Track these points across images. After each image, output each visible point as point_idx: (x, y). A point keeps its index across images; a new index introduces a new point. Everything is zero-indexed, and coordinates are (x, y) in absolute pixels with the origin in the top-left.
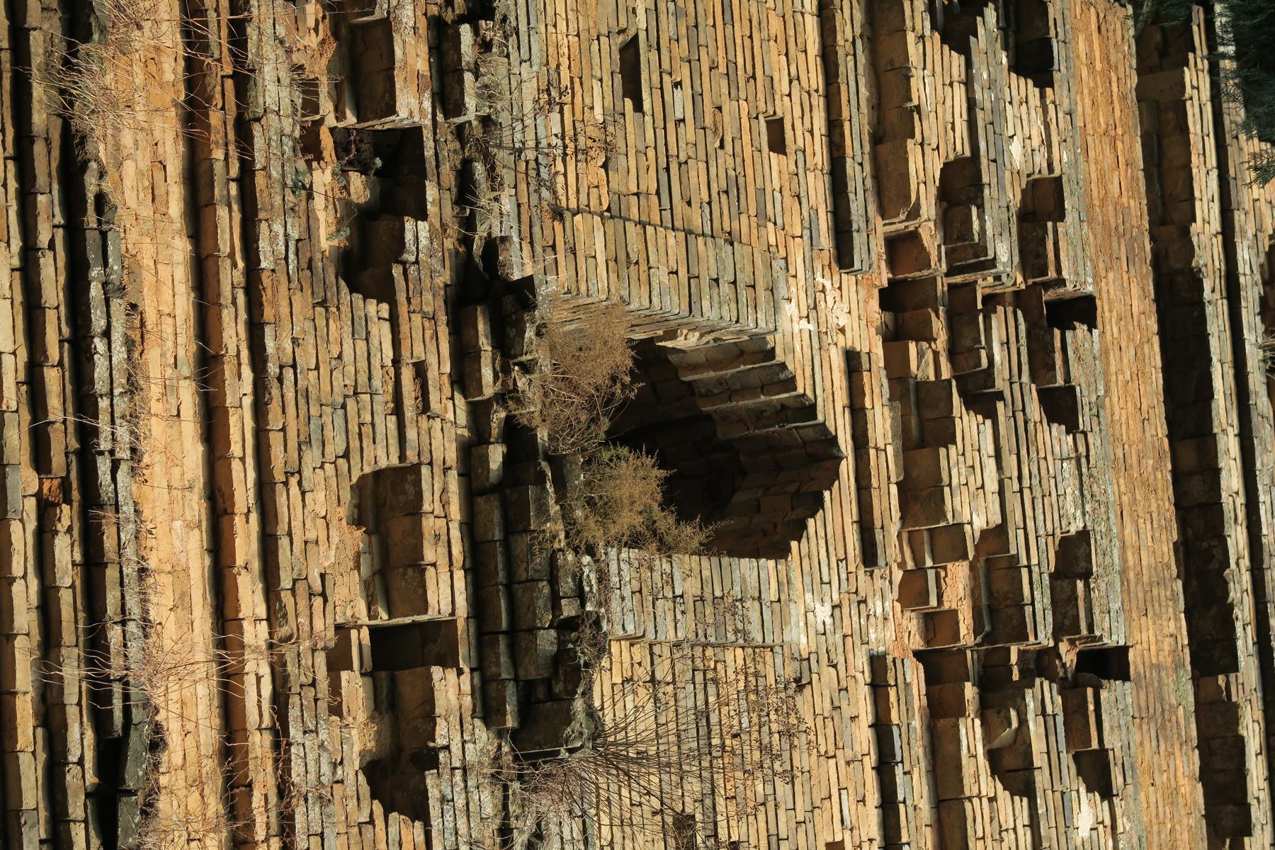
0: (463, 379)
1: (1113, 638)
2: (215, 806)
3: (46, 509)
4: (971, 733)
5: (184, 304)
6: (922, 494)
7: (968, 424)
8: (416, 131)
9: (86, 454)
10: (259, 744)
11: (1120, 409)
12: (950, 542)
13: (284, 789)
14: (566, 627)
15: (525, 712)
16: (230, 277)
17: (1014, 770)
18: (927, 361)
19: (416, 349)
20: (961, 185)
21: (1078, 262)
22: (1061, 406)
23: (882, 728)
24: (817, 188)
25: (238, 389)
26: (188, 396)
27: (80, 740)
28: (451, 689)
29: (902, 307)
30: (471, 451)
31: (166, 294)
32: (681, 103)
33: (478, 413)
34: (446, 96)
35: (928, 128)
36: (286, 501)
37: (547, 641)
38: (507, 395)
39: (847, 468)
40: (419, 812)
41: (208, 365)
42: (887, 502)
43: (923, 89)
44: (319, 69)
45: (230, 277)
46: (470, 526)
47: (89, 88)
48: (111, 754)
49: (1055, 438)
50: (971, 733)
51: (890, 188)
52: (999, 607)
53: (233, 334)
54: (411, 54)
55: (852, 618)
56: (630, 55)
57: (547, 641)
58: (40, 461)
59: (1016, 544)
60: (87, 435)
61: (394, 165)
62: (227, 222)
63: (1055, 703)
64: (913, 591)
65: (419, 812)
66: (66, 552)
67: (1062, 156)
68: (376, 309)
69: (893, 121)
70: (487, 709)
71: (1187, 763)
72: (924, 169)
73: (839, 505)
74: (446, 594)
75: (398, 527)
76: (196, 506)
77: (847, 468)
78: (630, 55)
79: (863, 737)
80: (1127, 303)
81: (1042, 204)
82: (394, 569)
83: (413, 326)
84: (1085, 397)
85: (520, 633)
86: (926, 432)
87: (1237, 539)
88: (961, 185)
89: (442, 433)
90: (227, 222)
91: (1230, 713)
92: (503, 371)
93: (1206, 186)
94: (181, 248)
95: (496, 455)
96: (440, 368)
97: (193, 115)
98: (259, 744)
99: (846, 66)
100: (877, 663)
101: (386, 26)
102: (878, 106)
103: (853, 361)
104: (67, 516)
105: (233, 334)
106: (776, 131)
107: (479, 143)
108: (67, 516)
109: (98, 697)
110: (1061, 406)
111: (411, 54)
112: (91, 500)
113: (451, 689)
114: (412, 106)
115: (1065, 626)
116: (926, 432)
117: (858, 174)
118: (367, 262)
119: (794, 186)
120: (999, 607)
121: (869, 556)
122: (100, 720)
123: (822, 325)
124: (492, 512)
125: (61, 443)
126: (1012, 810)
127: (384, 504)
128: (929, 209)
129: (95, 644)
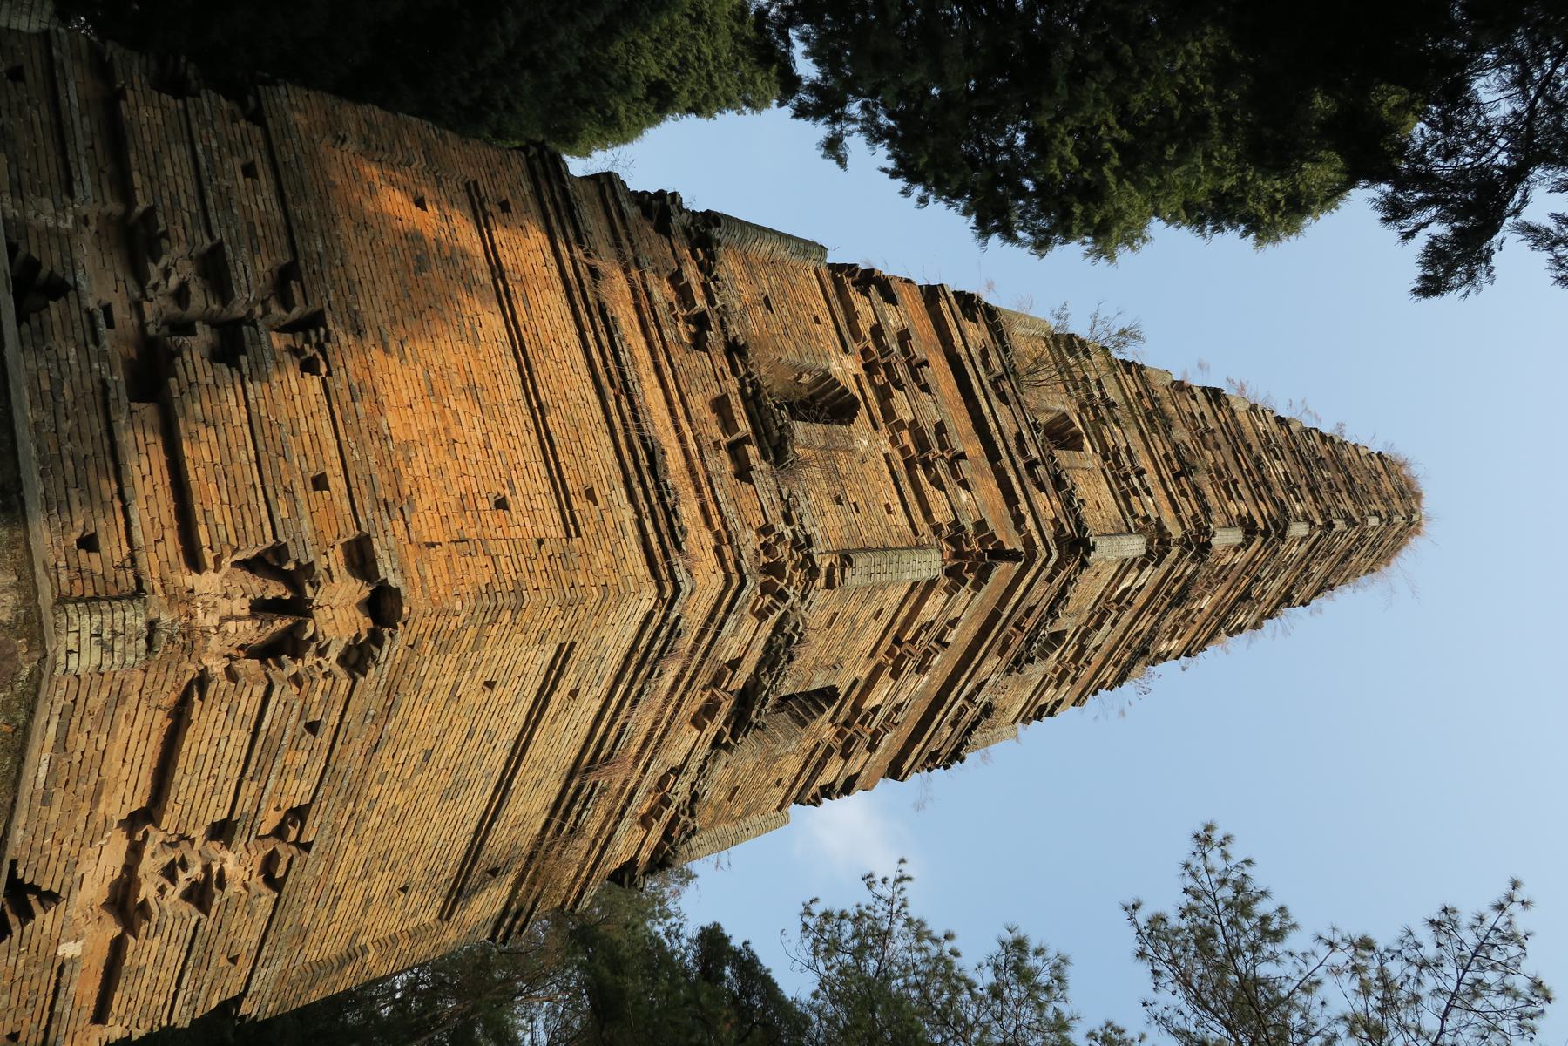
0: (735, 372)
1: (960, 449)
2: (689, 481)
3: (617, 398)
4: (921, 473)
5: (647, 354)
6: (888, 413)
7: (896, 393)
8: (704, 313)
9: (625, 382)
10: (697, 462)
11: (943, 388)
12: (901, 425)
13: (707, 471)
14: (780, 428)
15: (775, 455)
16: (658, 345)
17: (938, 484)
18: (880, 379)
19: (718, 364)
20: (877, 331)
21: (919, 352)
22: (925, 388)
23: (892, 473)
24: (833, 334)
25: (668, 373)
26: (654, 377)
27: (641, 454)
28: (752, 451)
29: (870, 368)
30: (742, 392)
31: (642, 353)
32: (785, 311)
33: (742, 381)
34: (711, 302)
35: (862, 316)
36: (689, 399)
37: (776, 433)
38: (749, 375)
39: (862, 405)
40: (750, 481)
41: (658, 369)
42: (877, 413)
43: (858, 306)
44: (673, 299)
45: (658, 345)
46: (747, 411)
47: (603, 292)
48: (651, 456)
49: (924, 396)
50: (921, 473)
51: (857, 335)
52: (922, 444)
53: (663, 359)
54: (698, 291)
55: (875, 445)
56: (766, 300)
57: (776, 433)
58: (613, 386)
59: (921, 424)
60: (623, 375)
61: (701, 321)
62: (654, 332)
63: (945, 466)
64: (894, 441)
65: (750, 481)
66: (625, 407)
67: (906, 323)
68: (704, 355)
69: (852, 317)
70: (764, 456)
71: (993, 484)
72: (865, 327)
73: (862, 413)
74: (744, 426)
75: (726, 412)
76: (664, 405)
77: (862, 405)
78: (766, 300)
79: (888, 476)
80: (974, 449)
81: (904, 337)
82: (728, 424)
83: (716, 358)
84: (932, 386)
85: (768, 433)
86: (884, 395)
87: (992, 425)
88: (877, 331)
89: (733, 385)
90: (654, 332)
91: (1004, 471)
92: (745, 367)
93: (955, 333)
94: (643, 340)
95: (749, 390)
96: (727, 369)
97: (638, 308)
98: (697, 462)
99: (833, 301)
100: (886, 456)
101: (688, 284)
102: (847, 314)
103: (856, 377)
104: (623, 398)
105: (663, 359)
106: (817, 320)
107: (723, 313)
108: (623, 398)
109: (643, 438)
110: (925, 388)
111: (698, 291)
112: (627, 389)
113: (752, 451)
114: (701, 304)
115: (943, 447)
116: (884, 395)
117: (847, 335)
118: (699, 343)
119: (826, 333)
120: (922, 444)
121: (876, 427)
122: (645, 446)
123: (845, 368)
124: (752, 405)
125: (617, 380)
126: (940, 495)
127: (720, 406)
128: (869, 337)
129: (639, 428)
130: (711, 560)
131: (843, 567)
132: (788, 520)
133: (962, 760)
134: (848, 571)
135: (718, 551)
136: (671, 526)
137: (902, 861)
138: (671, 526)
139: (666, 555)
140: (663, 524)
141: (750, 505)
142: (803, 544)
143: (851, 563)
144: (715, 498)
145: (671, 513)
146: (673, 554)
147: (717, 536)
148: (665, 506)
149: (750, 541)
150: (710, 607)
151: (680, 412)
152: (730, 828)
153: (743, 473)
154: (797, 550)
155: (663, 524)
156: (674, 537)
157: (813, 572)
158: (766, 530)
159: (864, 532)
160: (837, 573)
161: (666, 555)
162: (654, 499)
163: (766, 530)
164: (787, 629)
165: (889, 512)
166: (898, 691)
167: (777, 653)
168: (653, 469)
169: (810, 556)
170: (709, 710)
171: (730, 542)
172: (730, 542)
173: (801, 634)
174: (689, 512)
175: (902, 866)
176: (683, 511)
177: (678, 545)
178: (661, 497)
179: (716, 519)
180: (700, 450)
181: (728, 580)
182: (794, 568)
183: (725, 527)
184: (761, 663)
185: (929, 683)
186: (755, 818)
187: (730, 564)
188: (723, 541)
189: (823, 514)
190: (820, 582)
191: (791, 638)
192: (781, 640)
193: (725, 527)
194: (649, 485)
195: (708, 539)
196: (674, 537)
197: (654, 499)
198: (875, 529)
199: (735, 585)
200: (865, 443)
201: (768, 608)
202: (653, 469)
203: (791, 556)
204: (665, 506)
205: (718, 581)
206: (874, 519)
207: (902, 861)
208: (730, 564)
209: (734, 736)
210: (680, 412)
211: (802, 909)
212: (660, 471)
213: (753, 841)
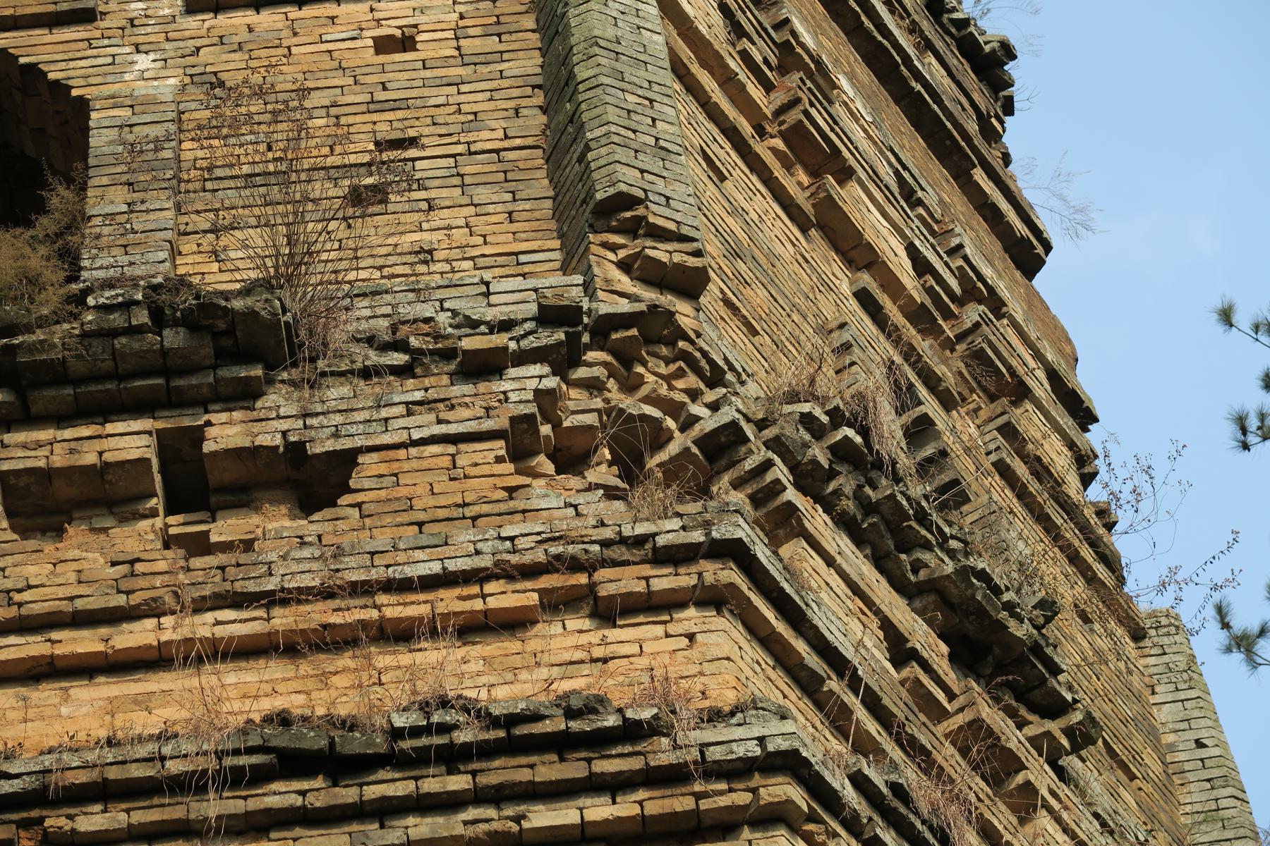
2: (346, 660)
10: (283, 619)
13: (326, 593)
14: (159, 319)
15: (248, 358)
28: (226, 431)
36: (36, 603)
37: (173, 338)
40: (348, 459)
46: (61, 420)
48: (294, 764)
57: (173, 338)
65: (348, 459)
70: (244, 396)
74: (130, 440)
75: (64, 491)
76: (45, 694)
82: (103, 495)
85: (167, 365)
98: (283, 619)
109: (237, 779)
113: (226, 431)
122: (260, 776)
130: (641, 640)
131: (635, 228)
132: (483, 367)
133: (1008, 52)
134: (658, 216)
135: (608, 612)
136: (561, 744)
137: (1226, 316)
138: (561, 744)
139: (672, 777)
140: (549, 770)
141: (437, 486)
142: (567, 332)
143: (627, 201)
144: (430, 583)
145: (513, 734)
146: (662, 753)
147: (556, 604)
148: (486, 751)
149: (568, 507)
150: (779, 677)
151: (84, 642)
152: (1194, 796)
153: (313, 480)
154: (576, 362)
155: (549, 770)
156: (601, 741)
157: (656, 329)
158: (519, 442)
159: (486, 138)
160: (661, 252)
161: (672, 777)
162: (458, 783)
163: (519, 442)
164: (819, 453)
165: (406, 43)
166: (875, 176)
167: (868, 508)
168: (339, 766)
169: (605, 326)
170: (998, 766)
171: (589, 567)
172: (589, 567)
173: (837, 418)
174: (496, 679)
175: (1243, 318)
176: (506, 695)
177: (632, 732)
178: (453, 758)
179: (503, 596)
180: (239, 601)
181: (714, 599)
182: (631, 385)
183: (531, 571)
184: (880, 562)
185: (851, 77)
186: (1164, 715)
187: (665, 580)
188: (575, 587)
189: (426, 254)
190: (684, 312)
191: (842, 452)
192: (846, 482)
193: (531, 571)
194: (402, 789)
195: (569, 635)
196: (601, 741)
197: (458, 783)
198: (475, 101)
199: (732, 575)
200: (144, 62)
201: (757, 500)
202: (339, 766)
203: (594, 386)
204: (486, 751)
205: (722, 634)
206: (439, 96)
207: (1226, 316)
208: (665, 580)
209: (1055, 708)
210: (84, 642)
211: (1238, 657)
212: (354, 744)
213: (1232, 733)
